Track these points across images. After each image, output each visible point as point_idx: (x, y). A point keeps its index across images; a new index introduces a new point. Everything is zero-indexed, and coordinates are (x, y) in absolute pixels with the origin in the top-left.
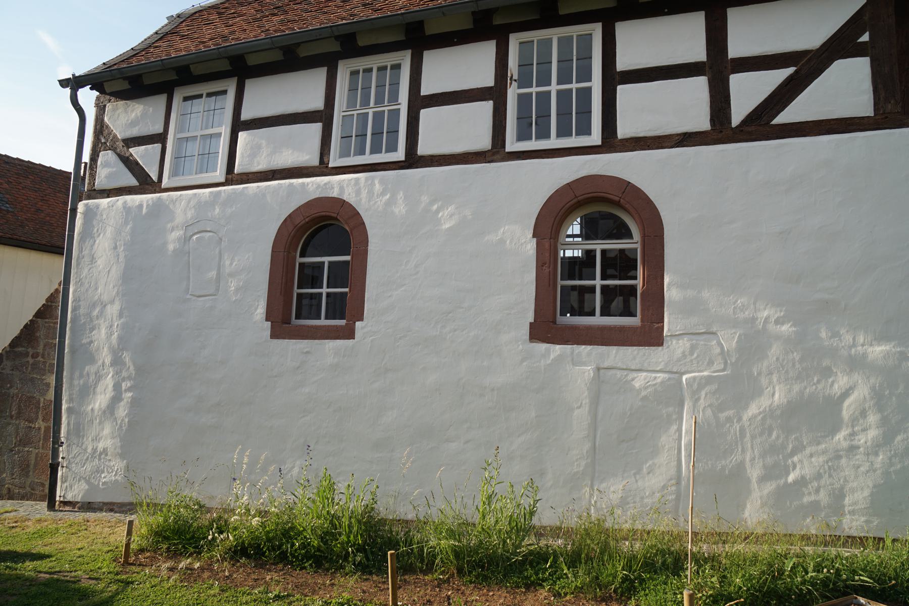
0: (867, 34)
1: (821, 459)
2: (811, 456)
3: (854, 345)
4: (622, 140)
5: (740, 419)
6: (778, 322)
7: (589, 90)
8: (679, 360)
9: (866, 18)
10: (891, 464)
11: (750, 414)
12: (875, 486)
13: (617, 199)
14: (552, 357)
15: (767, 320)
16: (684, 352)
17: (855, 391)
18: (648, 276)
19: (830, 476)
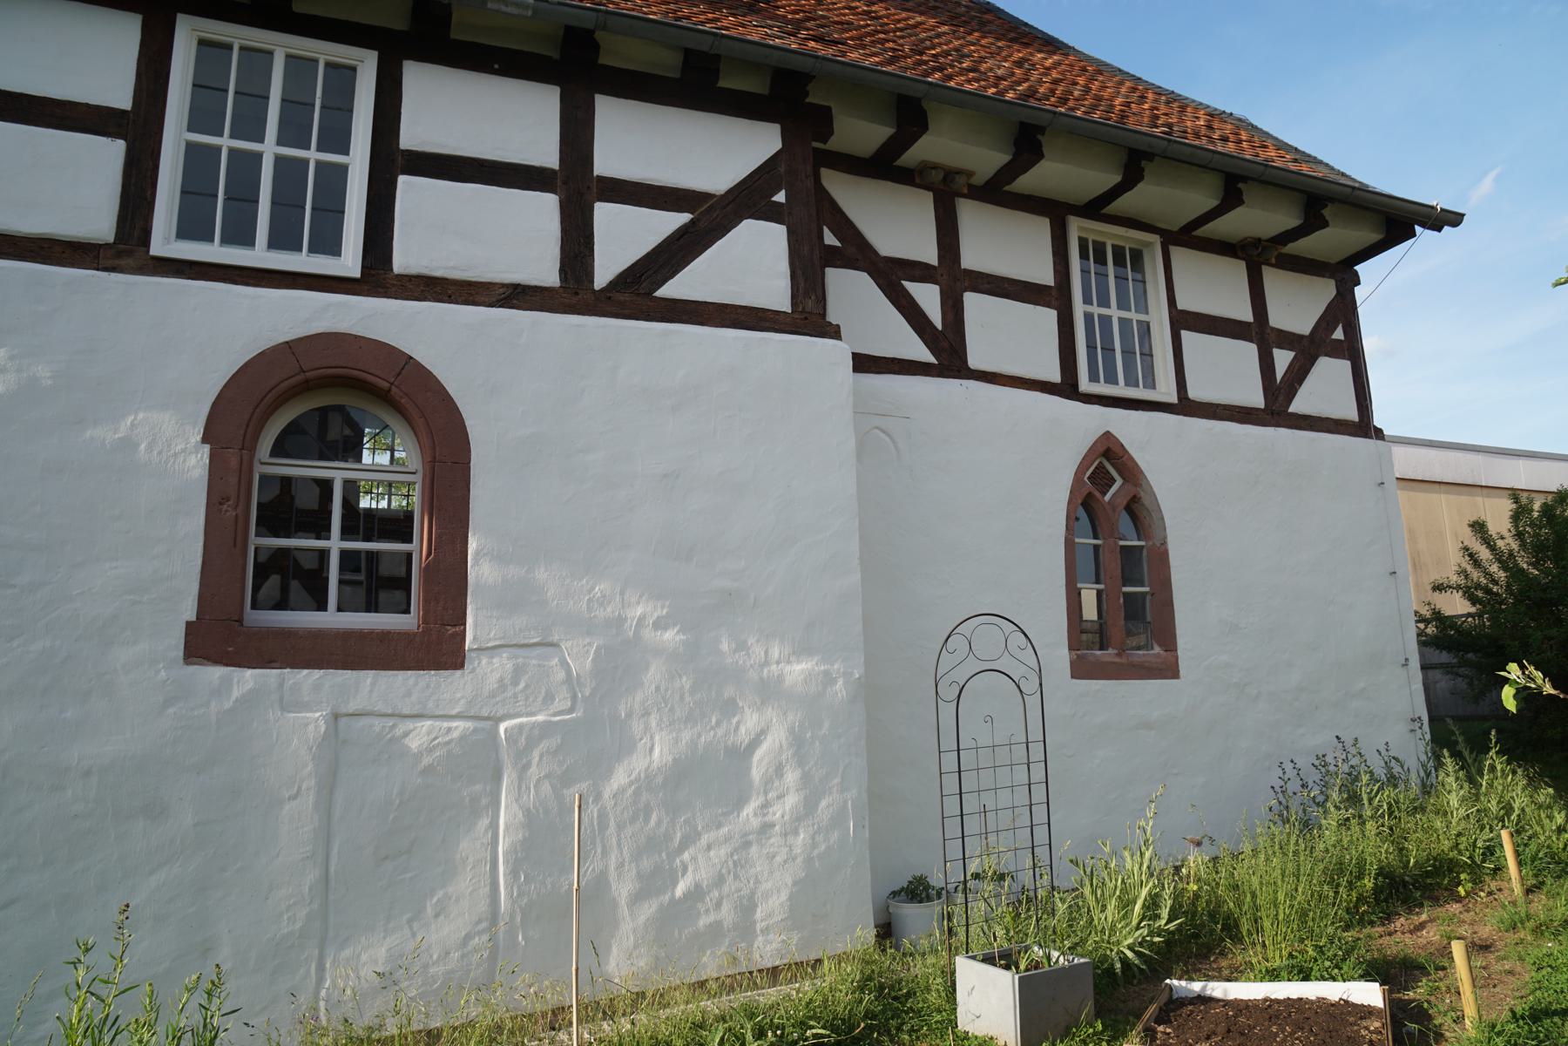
0: (783, 192)
1: (723, 852)
2: (709, 847)
3: (767, 663)
4: (400, 277)
5: (598, 797)
6: (659, 625)
7: (343, 170)
8: (492, 695)
9: (782, 169)
10: (814, 845)
11: (615, 787)
12: (795, 883)
13: (385, 385)
14: (236, 694)
15: (642, 619)
16: (501, 680)
17: (767, 733)
18: (439, 537)
19: (736, 877)
